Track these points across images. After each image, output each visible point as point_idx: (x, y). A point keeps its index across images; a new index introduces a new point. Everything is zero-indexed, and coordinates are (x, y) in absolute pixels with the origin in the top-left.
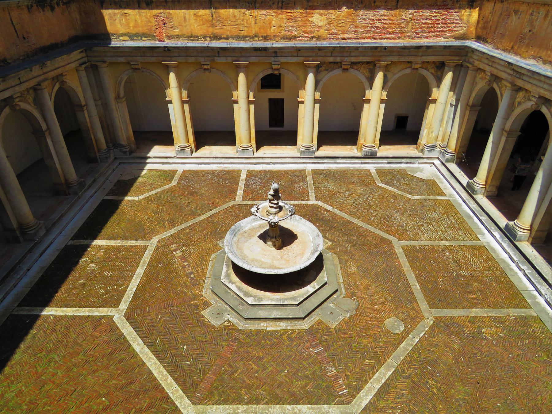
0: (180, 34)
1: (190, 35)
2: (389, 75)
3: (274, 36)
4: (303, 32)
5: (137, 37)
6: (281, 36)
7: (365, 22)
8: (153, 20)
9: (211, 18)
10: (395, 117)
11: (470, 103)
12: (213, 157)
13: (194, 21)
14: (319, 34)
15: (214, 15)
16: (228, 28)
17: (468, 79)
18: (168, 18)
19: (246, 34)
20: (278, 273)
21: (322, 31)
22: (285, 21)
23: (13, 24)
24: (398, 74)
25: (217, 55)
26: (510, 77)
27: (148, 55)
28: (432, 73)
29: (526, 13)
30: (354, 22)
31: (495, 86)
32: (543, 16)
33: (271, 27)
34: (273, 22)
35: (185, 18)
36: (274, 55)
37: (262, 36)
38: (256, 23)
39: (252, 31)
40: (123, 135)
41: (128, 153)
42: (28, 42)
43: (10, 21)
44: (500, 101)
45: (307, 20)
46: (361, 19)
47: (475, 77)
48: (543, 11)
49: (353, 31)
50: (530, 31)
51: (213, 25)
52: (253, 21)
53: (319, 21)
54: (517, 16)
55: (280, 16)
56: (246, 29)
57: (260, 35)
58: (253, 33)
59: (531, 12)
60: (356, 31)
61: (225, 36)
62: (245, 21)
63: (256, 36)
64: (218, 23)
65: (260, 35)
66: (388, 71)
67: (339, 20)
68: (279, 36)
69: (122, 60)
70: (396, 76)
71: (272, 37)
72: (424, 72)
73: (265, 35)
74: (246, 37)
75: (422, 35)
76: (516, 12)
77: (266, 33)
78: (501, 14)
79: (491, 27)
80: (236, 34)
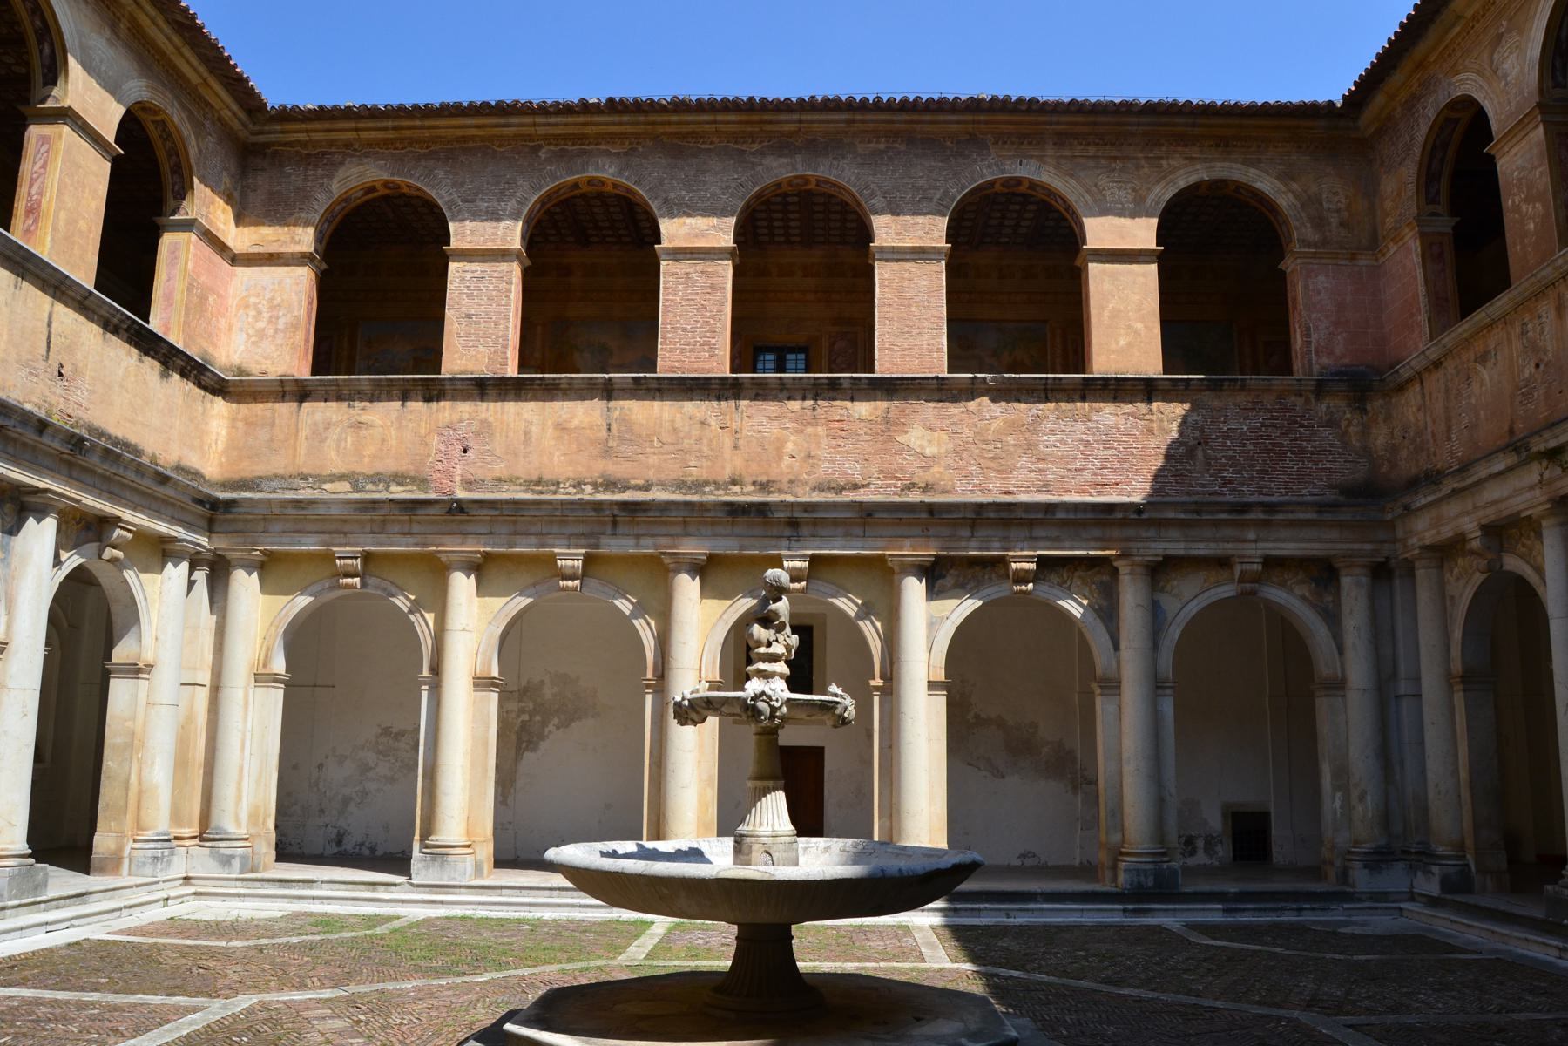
0: (505, 474)
1: (534, 478)
2: (1169, 604)
3: (791, 482)
4: (881, 472)
5: (373, 483)
6: (812, 483)
7: (1063, 448)
8: (435, 441)
9: (604, 434)
10: (1224, 815)
11: (1457, 667)
12: (551, 889)
13: (552, 442)
14: (931, 480)
15: (614, 427)
16: (653, 460)
17: (1424, 595)
18: (478, 434)
19: (705, 477)
20: (828, 877)
21: (936, 469)
22: (824, 441)
23: (49, 324)
24: (1190, 598)
25: (609, 531)
26: (1537, 492)
27: (397, 528)
28: (1303, 598)
29: (1509, 341)
30: (1030, 446)
31: (1512, 563)
32: (1553, 314)
33: (780, 459)
34: (790, 447)
35: (527, 433)
36: (788, 532)
37: (754, 483)
38: (736, 447)
39: (723, 468)
40: (239, 798)
41: (236, 863)
42: (66, 388)
43: (46, 315)
44: (1540, 591)
45: (891, 440)
46: (1053, 439)
47: (1442, 585)
48: (1546, 308)
49: (1031, 471)
50: (1537, 366)
51: (607, 452)
52: (727, 441)
53: (925, 443)
54: (1490, 364)
55: (810, 430)
56: (705, 463)
57: (748, 480)
58: (726, 476)
59: (1518, 330)
60: (1040, 471)
61: (641, 482)
62: (705, 441)
63: (734, 482)
64: (623, 448)
65: (748, 480)
66: (1162, 590)
67: (986, 442)
68: (805, 483)
69: (310, 545)
70: (1194, 608)
71: (785, 486)
72: (1275, 594)
73: (764, 479)
74: (707, 483)
75: (1242, 484)
76: (1483, 359)
77: (767, 474)
78: (1447, 391)
79: (1433, 435)
80: (673, 476)
